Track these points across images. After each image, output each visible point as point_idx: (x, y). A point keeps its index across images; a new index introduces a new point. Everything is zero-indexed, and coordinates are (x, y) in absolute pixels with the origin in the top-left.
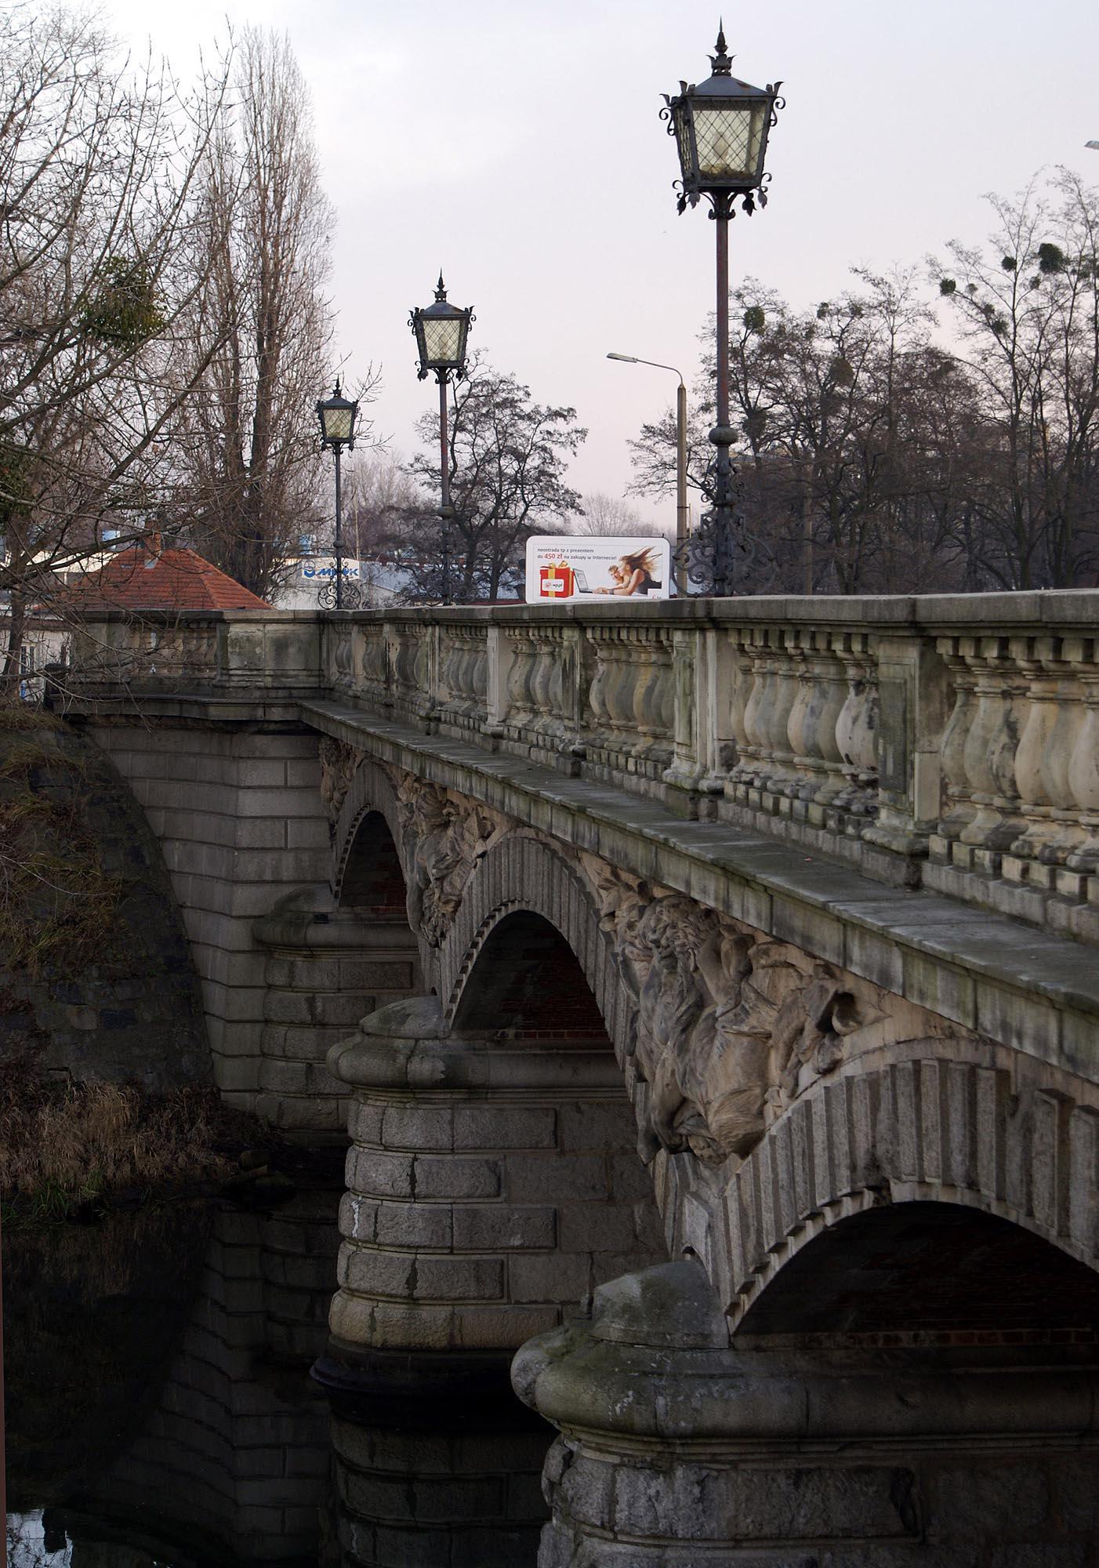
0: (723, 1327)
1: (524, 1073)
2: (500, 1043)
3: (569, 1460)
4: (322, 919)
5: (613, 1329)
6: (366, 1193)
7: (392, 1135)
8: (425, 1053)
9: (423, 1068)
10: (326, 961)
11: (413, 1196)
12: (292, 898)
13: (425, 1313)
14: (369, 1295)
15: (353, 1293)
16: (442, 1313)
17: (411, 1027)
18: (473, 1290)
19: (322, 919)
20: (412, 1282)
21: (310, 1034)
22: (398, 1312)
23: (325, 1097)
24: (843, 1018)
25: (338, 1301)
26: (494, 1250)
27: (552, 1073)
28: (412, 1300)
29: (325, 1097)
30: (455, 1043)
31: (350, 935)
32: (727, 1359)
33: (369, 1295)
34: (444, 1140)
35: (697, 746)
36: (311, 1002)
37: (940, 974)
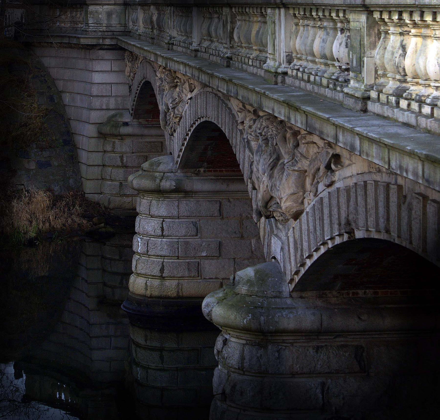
0: (288, 288)
1: (207, 186)
2: (197, 174)
3: (225, 342)
4: (126, 124)
5: (243, 289)
6: (143, 235)
7: (154, 211)
8: (168, 178)
9: (167, 184)
10: (128, 141)
11: (163, 236)
12: (114, 116)
13: (167, 283)
14: (145, 275)
15: (138, 275)
16: (174, 283)
17: (162, 168)
18: (186, 274)
19: (126, 124)
20: (162, 270)
21: (121, 171)
22: (156, 282)
23: (127, 196)
24: (335, 164)
25: (132, 278)
26: (195, 258)
27: (218, 186)
28: (162, 278)
29: (127, 196)
30: (180, 174)
31: (137, 131)
32: (289, 301)
33: (145, 275)
34: (175, 213)
35: (277, 55)
36: (122, 158)
37: (374, 146)
